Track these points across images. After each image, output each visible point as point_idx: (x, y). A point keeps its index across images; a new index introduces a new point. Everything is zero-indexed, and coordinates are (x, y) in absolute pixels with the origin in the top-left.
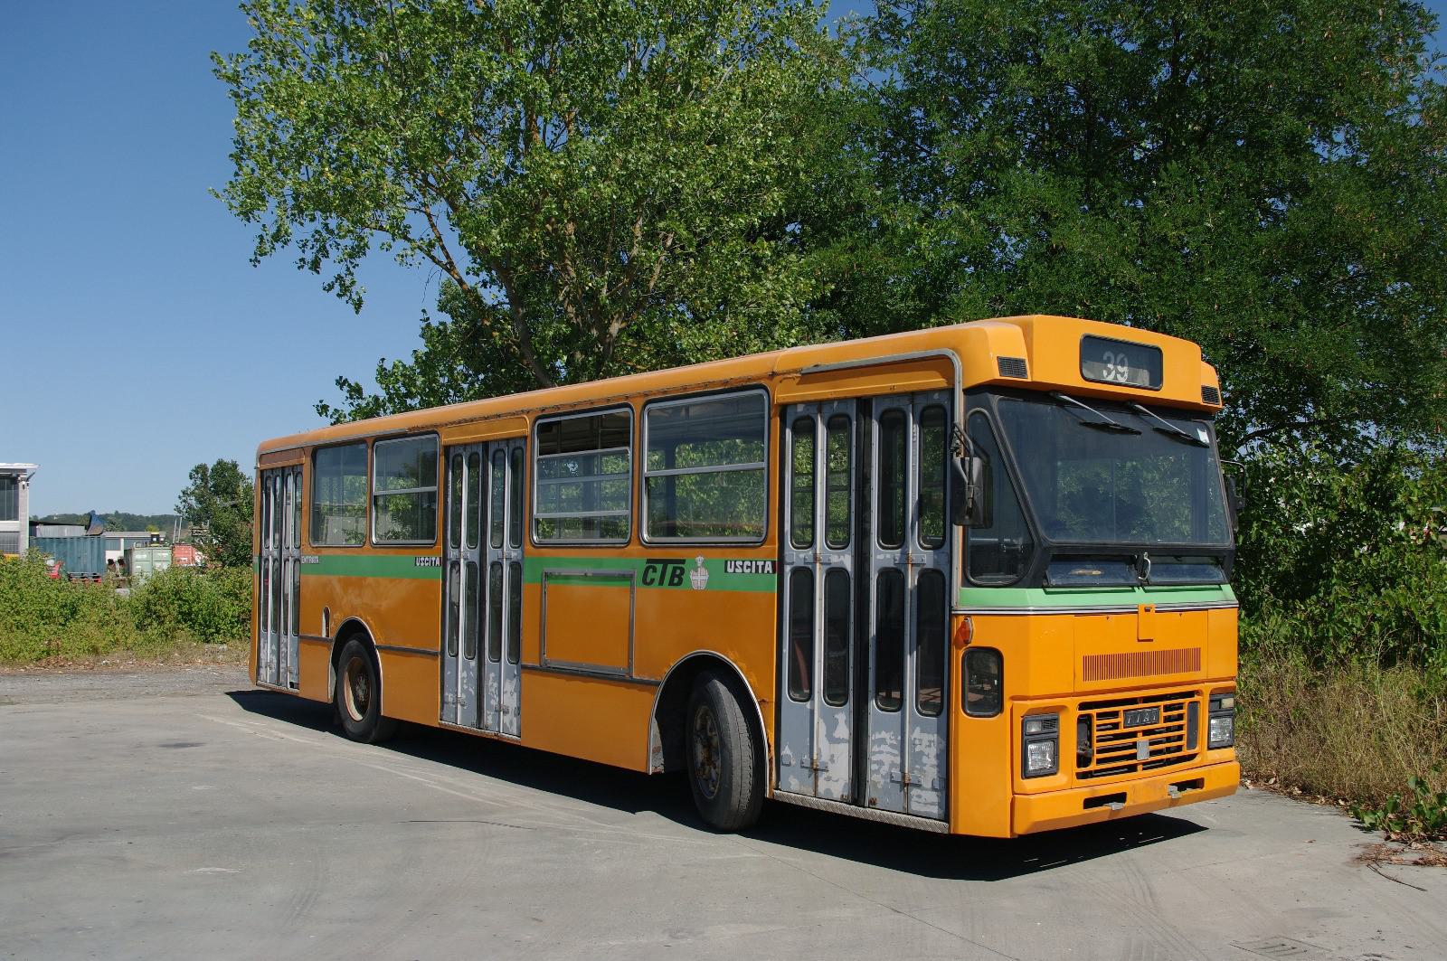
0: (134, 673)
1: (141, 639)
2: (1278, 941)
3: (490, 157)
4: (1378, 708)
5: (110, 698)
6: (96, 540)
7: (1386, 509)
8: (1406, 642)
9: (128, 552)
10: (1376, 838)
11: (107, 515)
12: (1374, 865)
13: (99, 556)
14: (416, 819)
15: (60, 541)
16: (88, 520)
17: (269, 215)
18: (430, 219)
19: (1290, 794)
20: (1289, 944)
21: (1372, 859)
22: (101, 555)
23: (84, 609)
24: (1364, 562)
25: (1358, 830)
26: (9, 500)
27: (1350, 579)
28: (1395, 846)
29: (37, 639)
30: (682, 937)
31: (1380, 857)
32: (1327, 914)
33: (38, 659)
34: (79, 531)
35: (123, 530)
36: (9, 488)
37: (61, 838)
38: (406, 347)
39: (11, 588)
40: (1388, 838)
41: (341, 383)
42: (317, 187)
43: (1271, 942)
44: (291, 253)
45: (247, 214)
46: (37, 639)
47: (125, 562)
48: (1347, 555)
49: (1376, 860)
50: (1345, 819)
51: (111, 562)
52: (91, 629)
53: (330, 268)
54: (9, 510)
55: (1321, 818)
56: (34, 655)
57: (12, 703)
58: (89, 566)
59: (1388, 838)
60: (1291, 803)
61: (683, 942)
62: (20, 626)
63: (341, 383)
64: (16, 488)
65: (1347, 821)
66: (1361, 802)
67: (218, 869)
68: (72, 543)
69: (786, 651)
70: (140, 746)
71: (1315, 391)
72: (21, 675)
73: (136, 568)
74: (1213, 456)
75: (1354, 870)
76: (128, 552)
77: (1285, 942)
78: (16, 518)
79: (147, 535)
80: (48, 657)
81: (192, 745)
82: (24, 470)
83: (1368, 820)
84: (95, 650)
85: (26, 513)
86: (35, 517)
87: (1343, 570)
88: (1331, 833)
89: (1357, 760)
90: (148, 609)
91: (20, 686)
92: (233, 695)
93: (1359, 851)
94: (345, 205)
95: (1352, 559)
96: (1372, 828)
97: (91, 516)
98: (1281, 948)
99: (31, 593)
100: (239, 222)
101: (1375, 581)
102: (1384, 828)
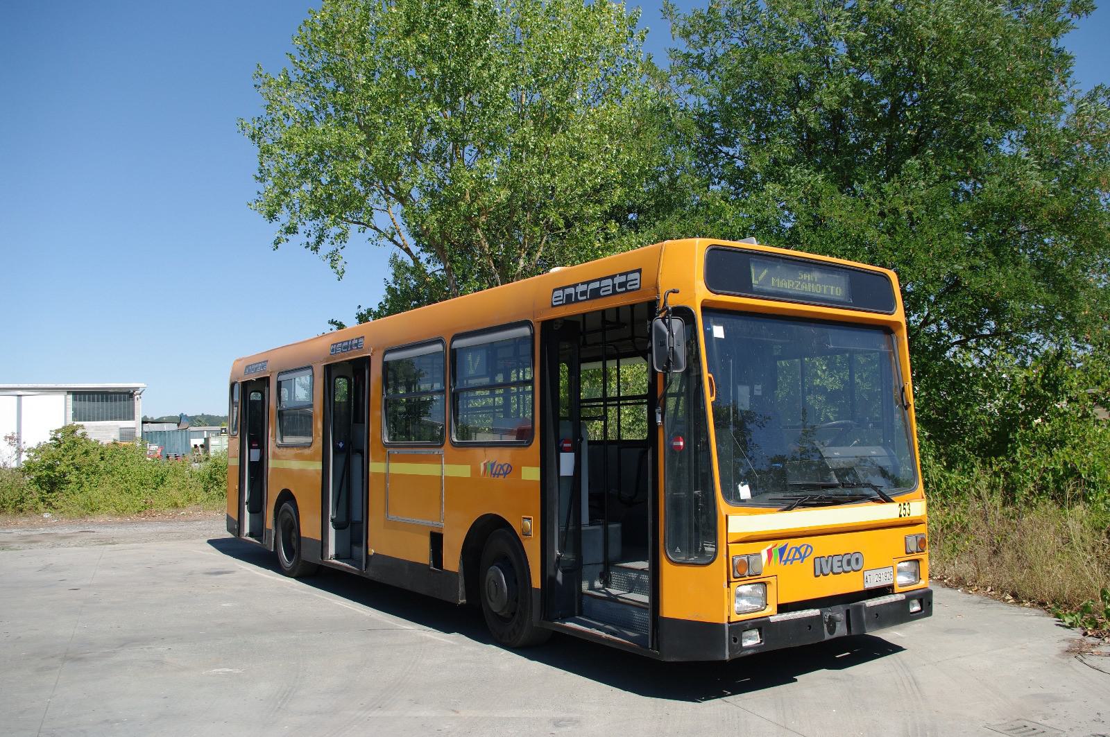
0: (199, 520)
1: (206, 497)
2: (1021, 723)
3: (426, 172)
4: (1057, 536)
5: (179, 538)
6: (184, 433)
7: (1055, 392)
8: (1065, 486)
9: (207, 440)
10: (1076, 634)
11: (197, 416)
12: (1080, 656)
13: (186, 443)
14: (371, 630)
15: (161, 433)
16: (179, 420)
17: (284, 216)
18: (388, 215)
19: (1005, 601)
20: (1031, 726)
21: (1077, 651)
22: (188, 443)
23: (169, 478)
24: (1039, 430)
25: (1061, 628)
26: (129, 407)
27: (1029, 442)
28: (1091, 640)
29: (138, 498)
30: (565, 726)
31: (1084, 649)
32: (1054, 699)
33: (139, 512)
34: (174, 427)
35: (206, 425)
36: (128, 400)
37: (122, 646)
38: (375, 297)
39: (122, 465)
40: (1085, 634)
41: (332, 322)
42: (320, 196)
43: (1016, 724)
44: (300, 238)
45: (272, 216)
46: (138, 498)
47: (205, 446)
48: (1027, 425)
49: (1080, 653)
50: (1049, 619)
51: (196, 446)
52: (173, 492)
53: (326, 247)
54: (129, 413)
55: (1031, 618)
56: (136, 510)
57: (113, 544)
58: (180, 449)
59: (1085, 634)
60: (1005, 607)
61: (563, 729)
62: (128, 491)
63: (332, 322)
64: (133, 400)
65: (1052, 620)
66: (1056, 605)
67: (228, 670)
68: (169, 434)
69: (650, 480)
70: (191, 573)
71: (997, 311)
72: (127, 523)
73: (212, 449)
74: (673, 451)
75: (1065, 661)
76: (207, 440)
77: (1027, 723)
78: (133, 419)
79: (219, 428)
80: (145, 511)
81: (226, 573)
82: (138, 388)
83: (1068, 620)
84: (176, 505)
85: (139, 416)
86: (145, 417)
87: (1023, 436)
88: (1043, 634)
89: (1056, 577)
90: (211, 478)
91: (131, 530)
92: (210, 542)
93: (1066, 645)
94: (339, 206)
95: (1031, 428)
96: (1072, 626)
97: (181, 417)
98: (1025, 729)
99: (136, 469)
100: (261, 220)
101: (1050, 444)
102: (1080, 626)
